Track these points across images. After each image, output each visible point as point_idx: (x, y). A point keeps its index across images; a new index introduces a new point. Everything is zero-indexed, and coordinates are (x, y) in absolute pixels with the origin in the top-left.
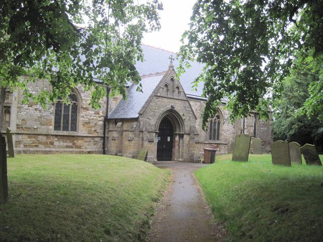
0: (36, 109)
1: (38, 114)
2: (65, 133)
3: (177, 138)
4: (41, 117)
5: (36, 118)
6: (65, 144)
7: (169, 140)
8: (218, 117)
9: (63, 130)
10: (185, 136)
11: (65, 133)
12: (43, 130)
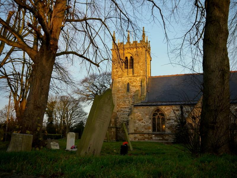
0: (142, 122)
1: (143, 124)
2: (158, 133)
4: (145, 126)
5: (143, 126)
6: (159, 138)
9: (157, 132)
11: (158, 133)
12: (146, 131)
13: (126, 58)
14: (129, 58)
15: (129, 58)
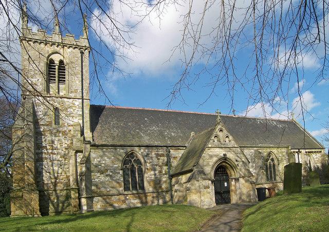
3: (233, 183)
7: (226, 184)
8: (272, 160)
10: (241, 180)
13: (52, 61)
14: (57, 62)
15: (57, 62)
